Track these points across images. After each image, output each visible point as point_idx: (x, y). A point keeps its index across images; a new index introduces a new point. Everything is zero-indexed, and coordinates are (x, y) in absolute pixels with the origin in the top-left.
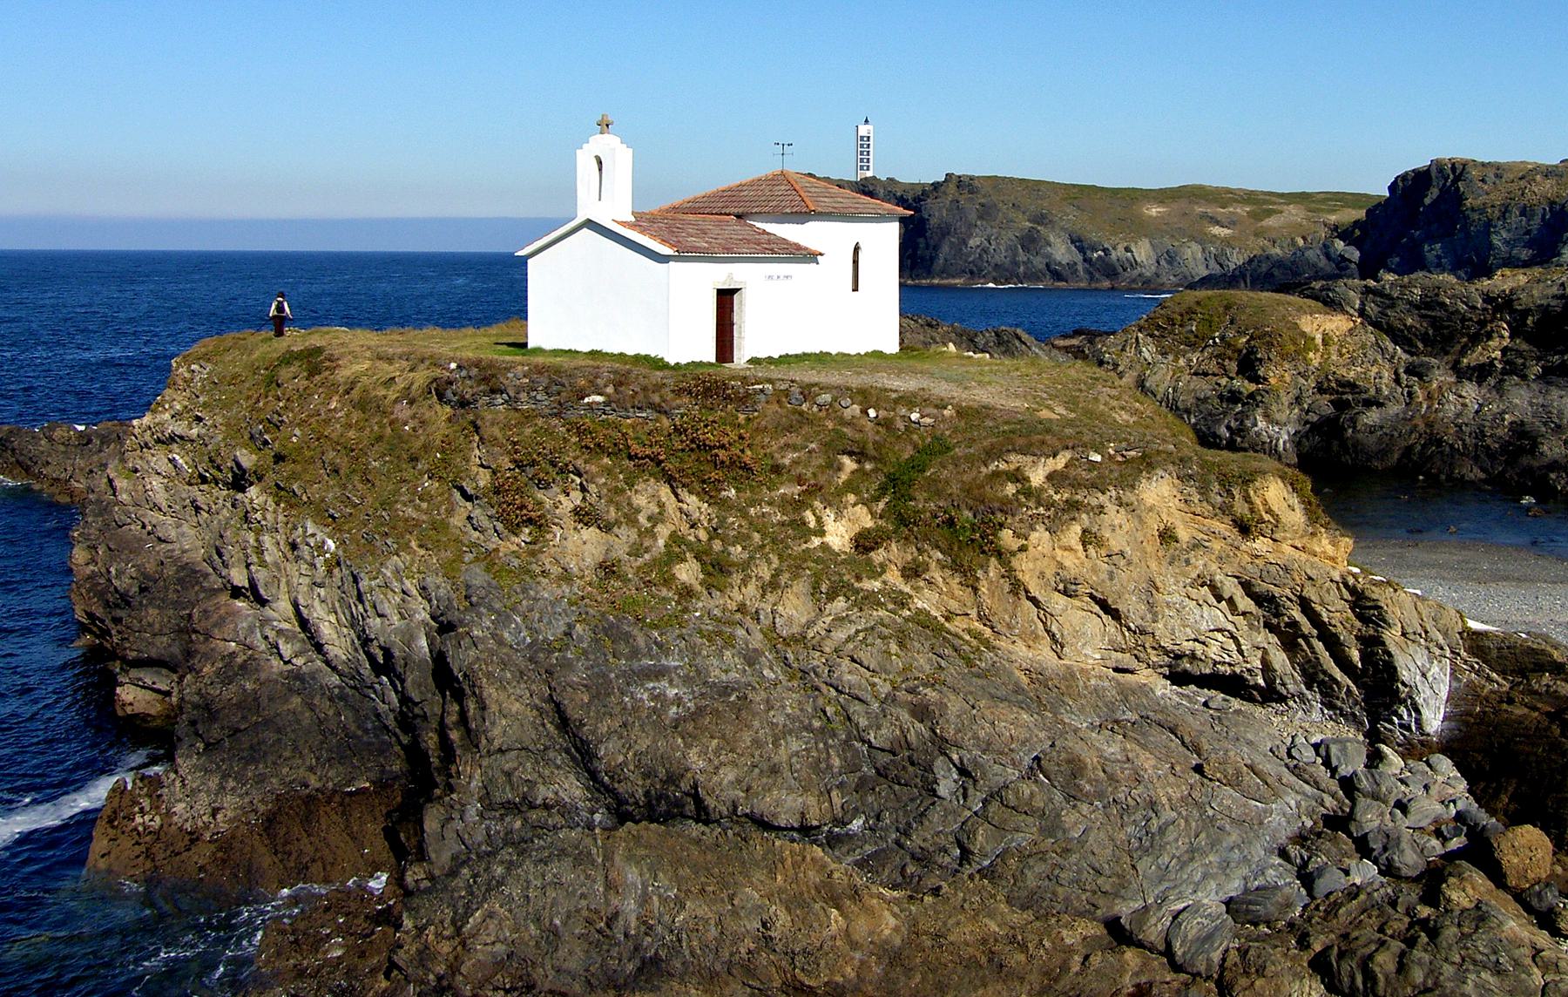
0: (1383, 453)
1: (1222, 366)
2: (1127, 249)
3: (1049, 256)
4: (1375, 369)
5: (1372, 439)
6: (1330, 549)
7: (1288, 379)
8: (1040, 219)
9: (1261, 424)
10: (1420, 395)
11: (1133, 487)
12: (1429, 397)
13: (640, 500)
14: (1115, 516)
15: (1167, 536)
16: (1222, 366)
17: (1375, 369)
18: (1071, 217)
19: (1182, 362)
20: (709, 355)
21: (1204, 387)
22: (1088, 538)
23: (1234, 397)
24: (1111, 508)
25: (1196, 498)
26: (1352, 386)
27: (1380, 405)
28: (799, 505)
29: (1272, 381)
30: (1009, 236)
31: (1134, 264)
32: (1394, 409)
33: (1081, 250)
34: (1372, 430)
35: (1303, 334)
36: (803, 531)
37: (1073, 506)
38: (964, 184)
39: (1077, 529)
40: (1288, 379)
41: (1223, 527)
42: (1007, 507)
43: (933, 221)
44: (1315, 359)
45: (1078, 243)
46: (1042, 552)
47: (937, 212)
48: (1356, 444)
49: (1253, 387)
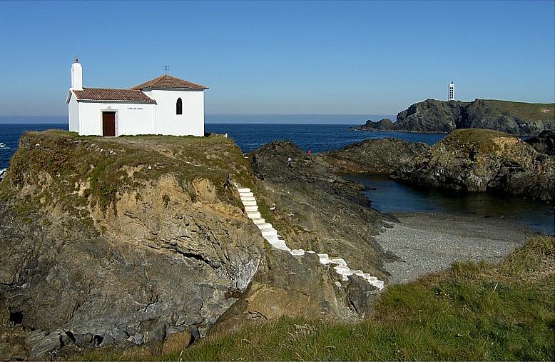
0: (518, 189)
1: (464, 155)
2: (534, 123)
3: (507, 125)
4: (526, 158)
5: (516, 183)
6: (222, 209)
7: (485, 160)
8: (505, 114)
9: (472, 176)
10: (540, 168)
11: (157, 179)
12: (543, 169)
13: (40, 177)
14: (149, 189)
15: (166, 199)
16: (464, 155)
17: (526, 158)
18: (516, 113)
19: (453, 153)
20: (98, 131)
21: (458, 162)
22: (138, 197)
23: (464, 166)
24: (149, 186)
25: (178, 185)
26: (516, 164)
27: (523, 171)
28: (76, 179)
29: (479, 161)
30: (494, 119)
31: (536, 128)
32: (528, 173)
33: (518, 123)
34: (517, 180)
35: (495, 144)
36: (73, 189)
37: (137, 184)
38: (481, 102)
39: (135, 193)
40: (485, 160)
41: (186, 196)
42: (120, 183)
43: (470, 114)
44: (499, 153)
45: (517, 121)
46: (127, 200)
47: (471, 111)
48: (510, 184)
49: (471, 162)
